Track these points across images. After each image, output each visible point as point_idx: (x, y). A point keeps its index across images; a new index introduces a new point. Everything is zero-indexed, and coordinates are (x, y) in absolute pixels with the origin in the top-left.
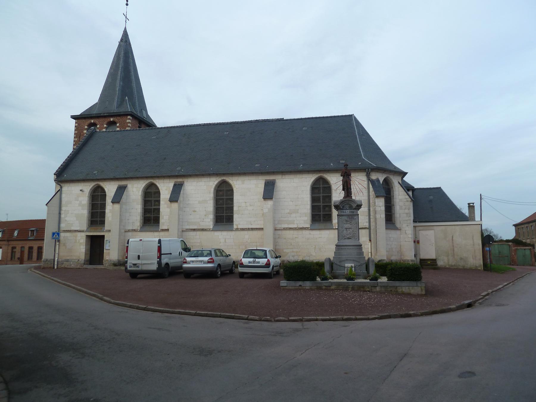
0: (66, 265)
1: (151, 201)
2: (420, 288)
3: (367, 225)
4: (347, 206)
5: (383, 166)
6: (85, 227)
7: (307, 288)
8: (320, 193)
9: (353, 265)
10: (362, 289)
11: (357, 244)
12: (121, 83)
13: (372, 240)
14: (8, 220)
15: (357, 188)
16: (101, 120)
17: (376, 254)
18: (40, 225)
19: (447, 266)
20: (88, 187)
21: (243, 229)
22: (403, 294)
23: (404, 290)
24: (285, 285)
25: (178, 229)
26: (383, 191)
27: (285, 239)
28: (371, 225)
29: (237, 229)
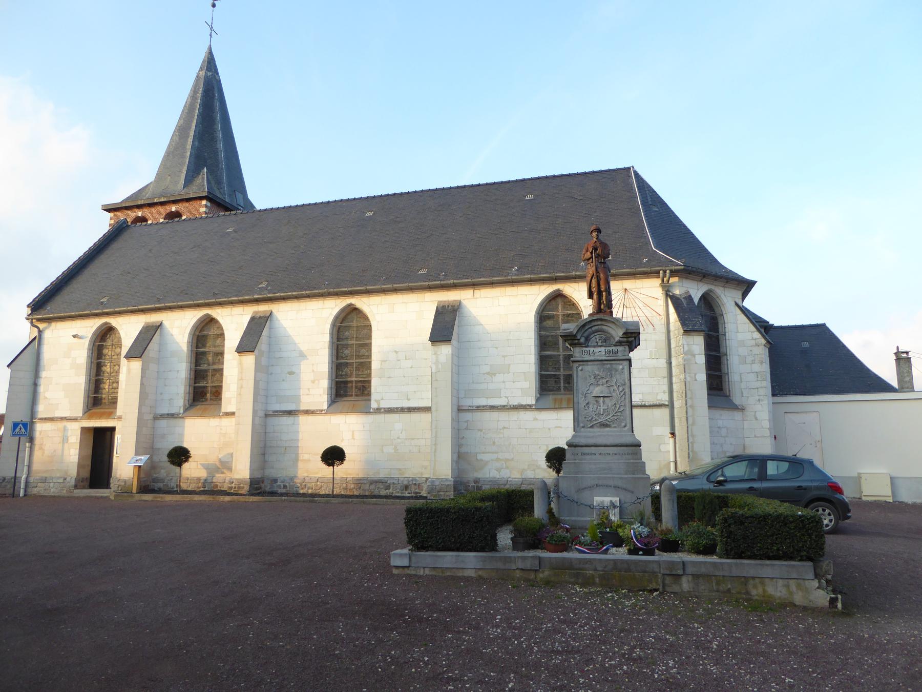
5: (699, 264)
6: (79, 412)
7: (471, 573)
9: (616, 500)
11: (627, 440)
12: (197, 143)
20: (88, 327)
21: (390, 411)
23: (770, 590)
24: (406, 562)
26: (700, 320)
27: (481, 430)
29: (378, 411)
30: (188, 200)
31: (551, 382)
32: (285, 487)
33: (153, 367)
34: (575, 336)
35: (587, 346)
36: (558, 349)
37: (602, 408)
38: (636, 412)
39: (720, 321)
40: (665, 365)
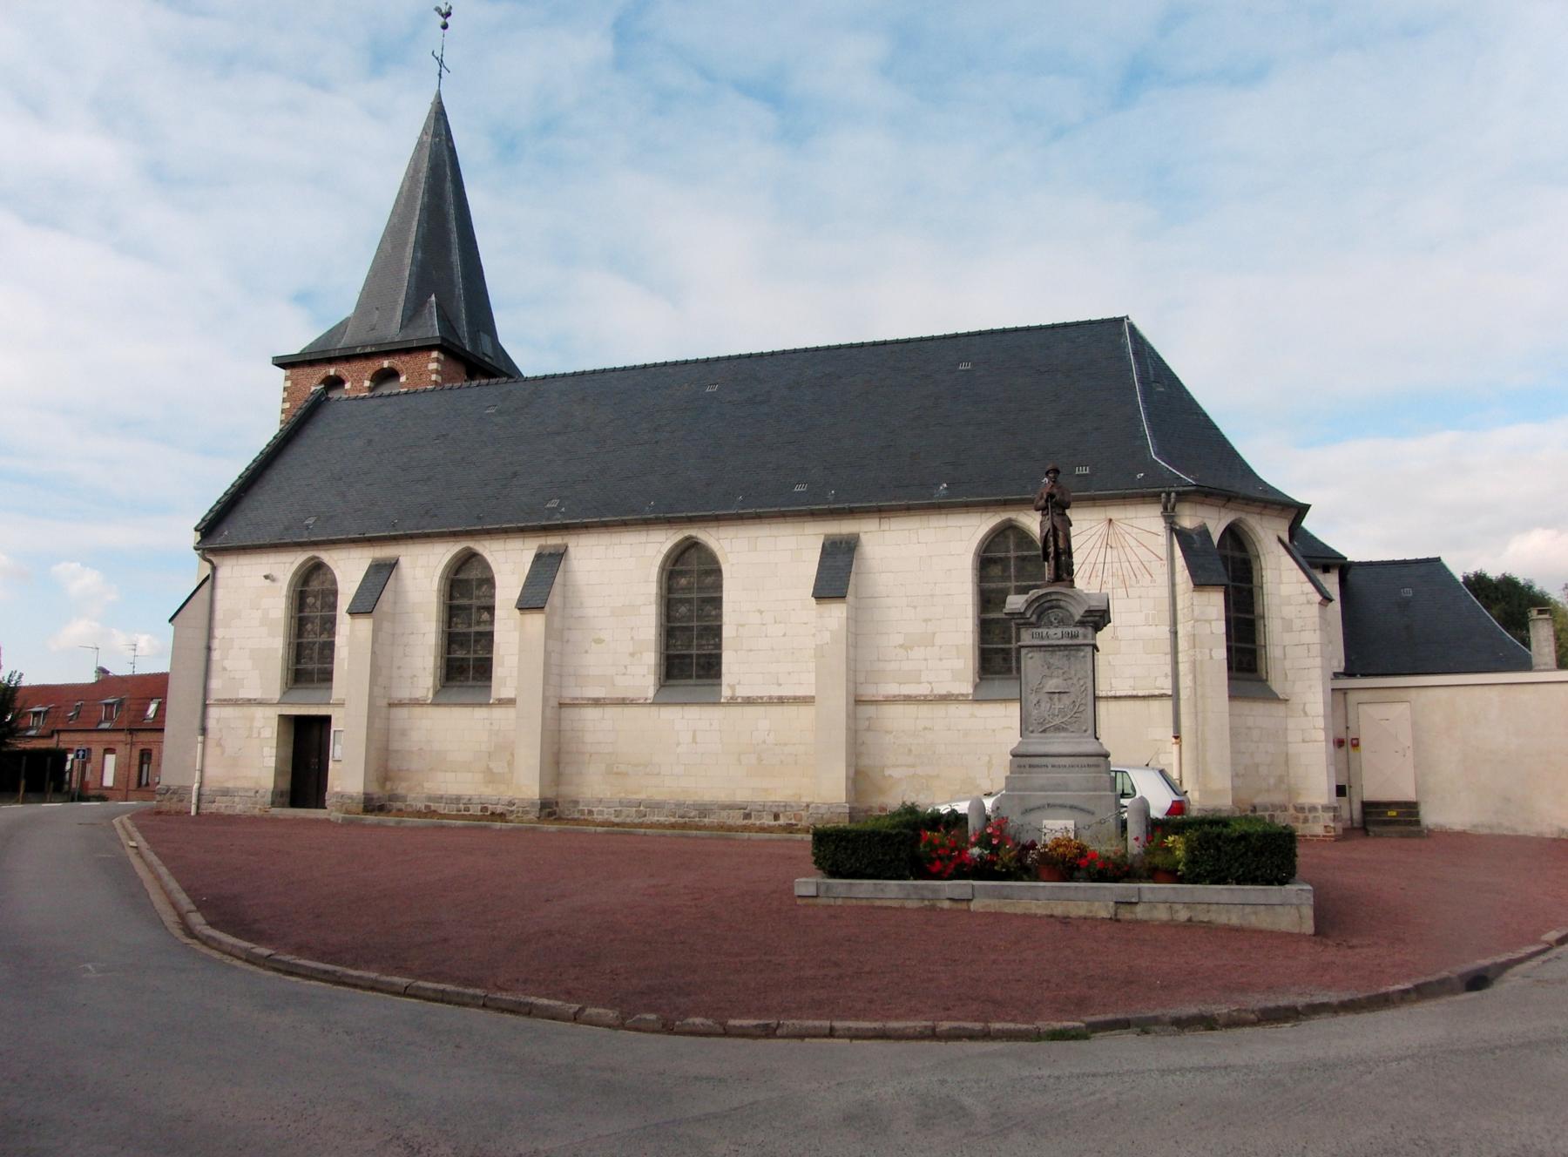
0: (220, 806)
1: (468, 608)
6: (275, 692)
8: (1008, 578)
11: (1089, 746)
14: (140, 671)
15: (1133, 558)
16: (357, 366)
18: (156, 686)
20: (286, 566)
21: (749, 701)
24: (812, 891)
25: (545, 700)
29: (732, 702)
30: (408, 351)
31: (998, 659)
32: (591, 812)
33: (386, 625)
38: (1102, 707)
39: (1255, 567)
40: (1168, 635)
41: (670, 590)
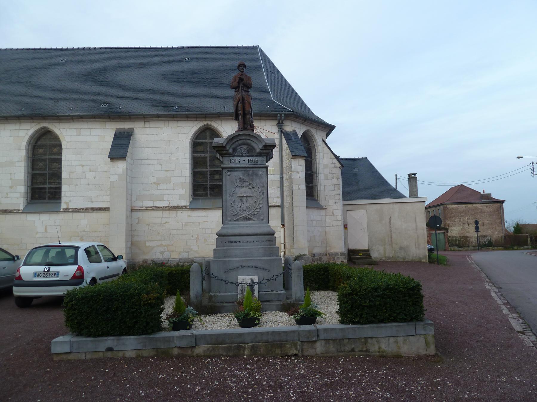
2: (422, 340)
3: (278, 201)
4: (243, 149)
7: (129, 354)
9: (255, 278)
10: (278, 351)
11: (264, 230)
13: (286, 225)
17: (292, 246)
19: (384, 259)
21: (77, 210)
22: (384, 358)
23: (384, 347)
24: (67, 349)
28: (285, 201)
29: (67, 210)
34: (225, 147)
35: (234, 156)
36: (206, 167)
37: (245, 205)
39: (313, 151)
40: (279, 179)
41: (33, 154)
